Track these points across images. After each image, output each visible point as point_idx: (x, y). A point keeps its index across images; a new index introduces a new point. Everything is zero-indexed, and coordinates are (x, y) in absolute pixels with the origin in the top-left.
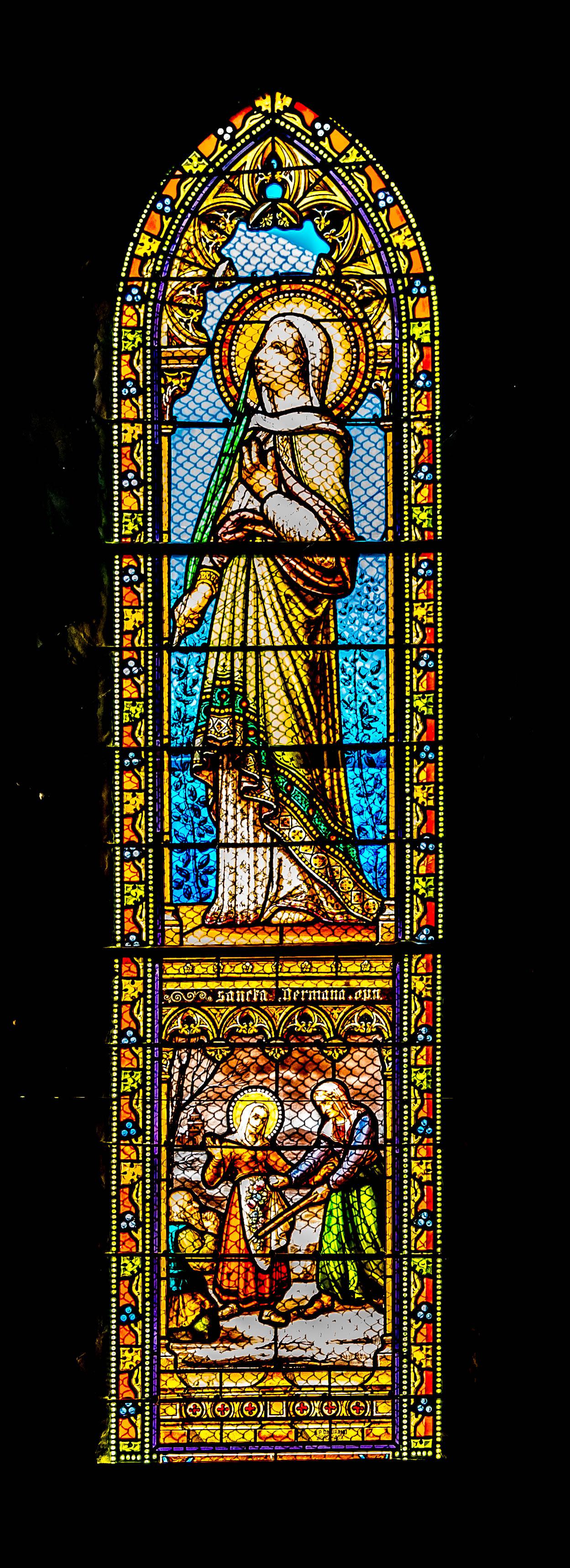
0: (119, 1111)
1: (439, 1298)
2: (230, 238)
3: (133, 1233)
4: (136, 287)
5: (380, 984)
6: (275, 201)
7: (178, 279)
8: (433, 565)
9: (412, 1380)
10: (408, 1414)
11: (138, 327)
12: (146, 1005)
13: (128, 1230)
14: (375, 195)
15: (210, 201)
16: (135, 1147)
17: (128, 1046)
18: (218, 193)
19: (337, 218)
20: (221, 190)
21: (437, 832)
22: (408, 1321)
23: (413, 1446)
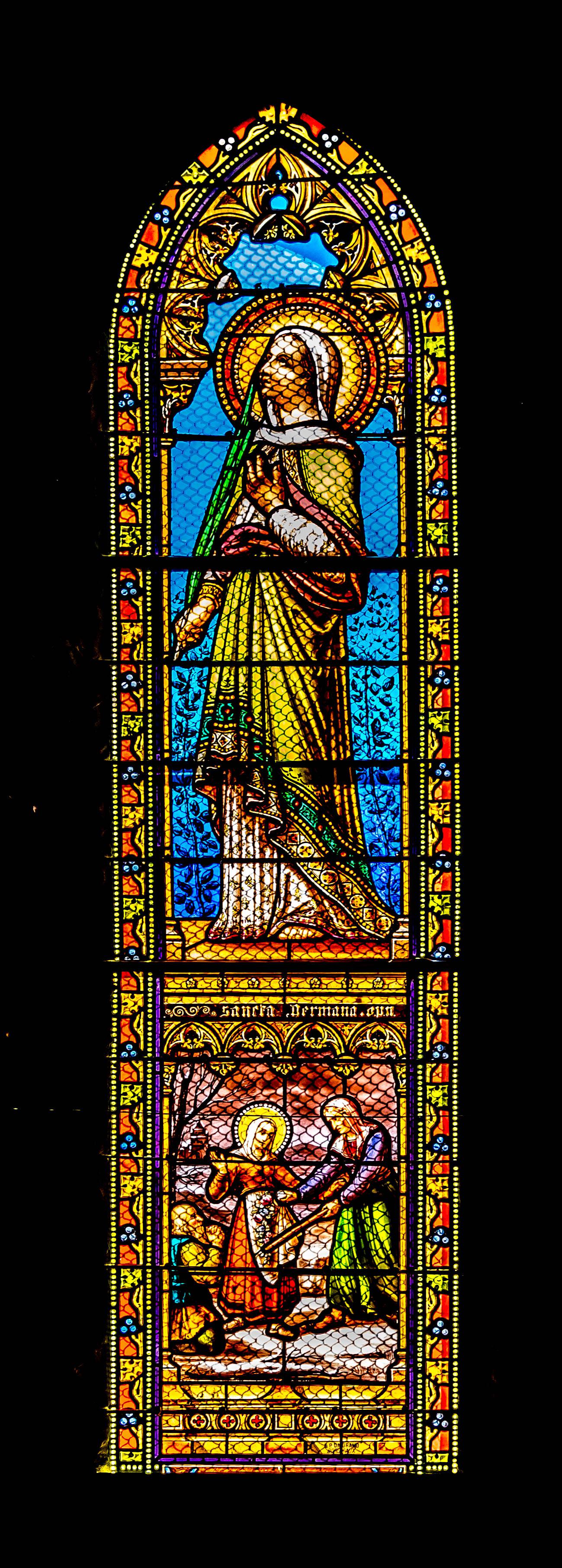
0: (118, 1124)
1: (454, 472)
2: (233, 249)
3: (134, 1245)
4: (133, 298)
5: (393, 1001)
6: (280, 213)
7: (177, 290)
8: (448, 582)
9: (427, 1395)
10: (423, 1428)
11: (135, 339)
12: (146, 1019)
13: (128, 1242)
14: (386, 208)
15: (211, 212)
16: (136, 1160)
17: (128, 1060)
18: (220, 204)
19: (346, 231)
20: (223, 201)
21: (454, 850)
22: (423, 1336)
23: (428, 1460)
